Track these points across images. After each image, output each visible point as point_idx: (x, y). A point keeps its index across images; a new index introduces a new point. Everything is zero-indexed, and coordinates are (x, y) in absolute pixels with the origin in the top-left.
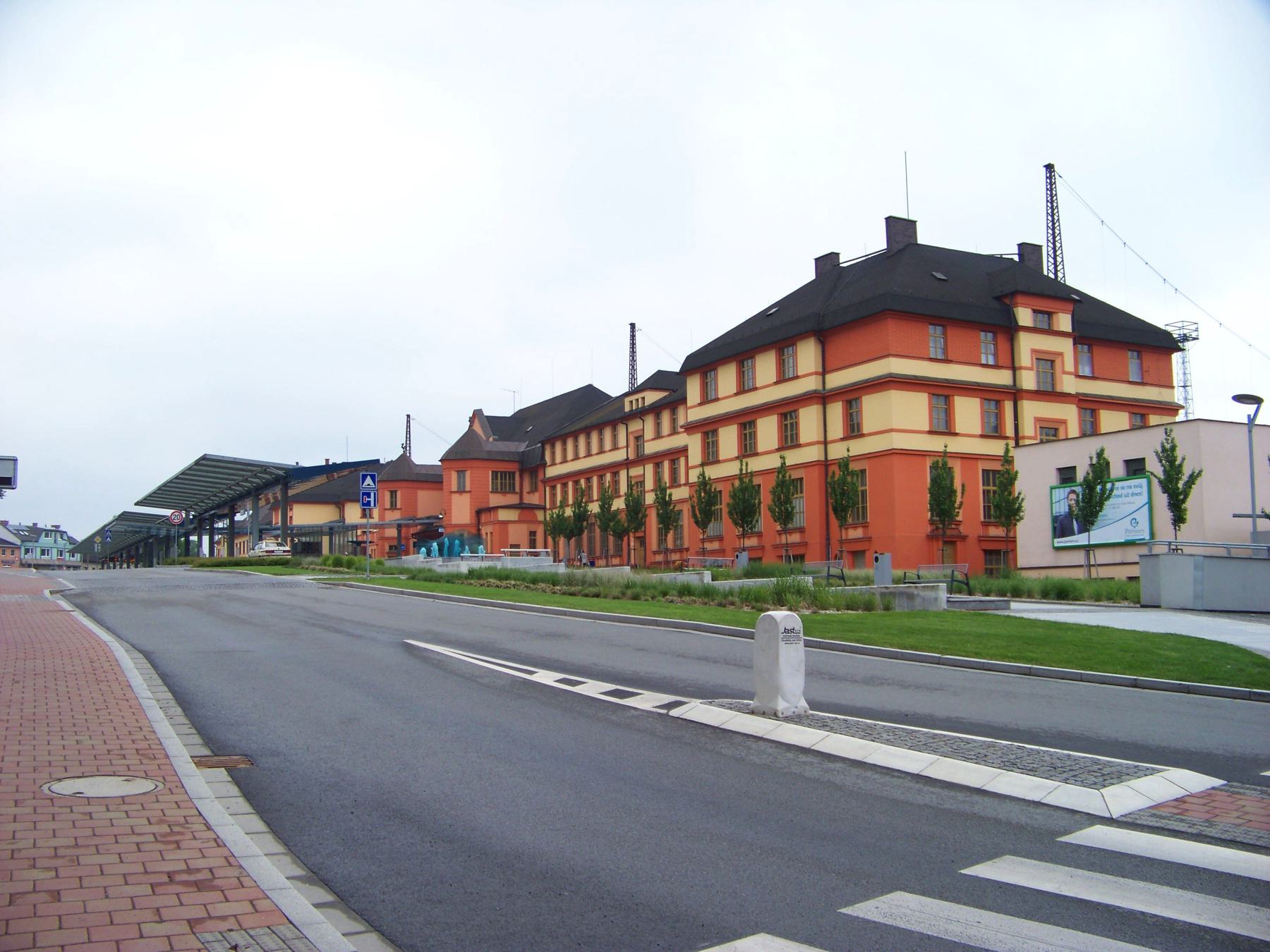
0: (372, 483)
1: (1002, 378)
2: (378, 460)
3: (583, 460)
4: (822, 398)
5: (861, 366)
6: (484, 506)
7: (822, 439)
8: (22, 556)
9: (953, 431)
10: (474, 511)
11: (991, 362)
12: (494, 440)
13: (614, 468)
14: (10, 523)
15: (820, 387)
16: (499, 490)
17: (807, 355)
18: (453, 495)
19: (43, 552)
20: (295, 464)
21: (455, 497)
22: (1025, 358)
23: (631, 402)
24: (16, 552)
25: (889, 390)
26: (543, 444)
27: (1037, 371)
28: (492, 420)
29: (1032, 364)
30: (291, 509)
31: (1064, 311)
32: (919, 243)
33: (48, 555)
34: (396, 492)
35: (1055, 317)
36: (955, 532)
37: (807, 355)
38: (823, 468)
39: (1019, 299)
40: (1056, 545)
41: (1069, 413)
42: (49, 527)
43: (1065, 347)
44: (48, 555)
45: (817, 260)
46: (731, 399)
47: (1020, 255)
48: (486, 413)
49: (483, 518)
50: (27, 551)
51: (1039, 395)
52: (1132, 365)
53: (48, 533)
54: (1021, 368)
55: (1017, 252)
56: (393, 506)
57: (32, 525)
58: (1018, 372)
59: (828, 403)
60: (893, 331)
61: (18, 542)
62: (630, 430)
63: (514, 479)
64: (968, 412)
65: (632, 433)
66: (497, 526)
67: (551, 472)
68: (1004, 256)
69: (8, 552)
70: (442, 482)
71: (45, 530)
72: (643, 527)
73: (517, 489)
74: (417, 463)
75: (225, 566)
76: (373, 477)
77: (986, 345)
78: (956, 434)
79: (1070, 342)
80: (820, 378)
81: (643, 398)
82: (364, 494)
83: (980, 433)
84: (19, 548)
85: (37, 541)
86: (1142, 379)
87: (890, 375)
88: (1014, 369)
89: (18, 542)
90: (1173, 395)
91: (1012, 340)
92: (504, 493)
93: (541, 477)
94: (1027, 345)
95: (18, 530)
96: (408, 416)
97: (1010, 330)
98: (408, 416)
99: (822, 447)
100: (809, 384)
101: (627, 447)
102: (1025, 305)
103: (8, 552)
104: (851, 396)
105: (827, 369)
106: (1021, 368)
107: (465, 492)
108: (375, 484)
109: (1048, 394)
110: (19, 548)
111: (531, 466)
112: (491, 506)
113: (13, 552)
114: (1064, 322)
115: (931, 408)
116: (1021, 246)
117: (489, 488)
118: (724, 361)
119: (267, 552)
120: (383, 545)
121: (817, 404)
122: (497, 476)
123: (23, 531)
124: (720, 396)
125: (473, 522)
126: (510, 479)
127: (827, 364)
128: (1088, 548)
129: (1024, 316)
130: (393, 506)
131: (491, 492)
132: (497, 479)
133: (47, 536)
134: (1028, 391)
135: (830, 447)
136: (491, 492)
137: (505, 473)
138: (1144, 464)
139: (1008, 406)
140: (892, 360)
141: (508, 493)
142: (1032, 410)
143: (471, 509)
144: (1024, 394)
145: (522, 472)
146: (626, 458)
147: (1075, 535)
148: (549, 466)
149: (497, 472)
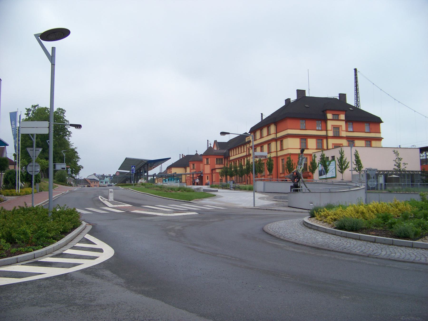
0: (134, 168)
1: (323, 133)
3: (235, 156)
4: (276, 140)
6: (213, 168)
7: (276, 151)
8: (100, 184)
9: (307, 148)
10: (211, 170)
11: (320, 129)
12: (219, 149)
13: (243, 157)
14: (96, 174)
15: (275, 137)
16: (218, 163)
17: (273, 128)
18: (205, 165)
19: (106, 183)
21: (206, 166)
22: (329, 127)
23: (247, 139)
24: (98, 183)
25: (288, 138)
26: (229, 150)
27: (334, 131)
28: (219, 143)
29: (332, 129)
30: (171, 169)
31: (342, 114)
32: (306, 96)
33: (107, 183)
34: (194, 164)
35: (339, 116)
36: (307, 175)
37: (273, 128)
38: (276, 158)
39: (328, 112)
40: (320, 178)
41: (344, 142)
42: (108, 175)
43: (343, 124)
44: (107, 183)
45: (285, 100)
46: (266, 137)
47: (339, 97)
48: (218, 141)
49: (213, 171)
50: (101, 182)
51: (333, 137)
52: (367, 127)
53: (107, 177)
54: (328, 130)
55: (339, 96)
56: (194, 169)
57: (103, 175)
58: (328, 131)
59: (300, 139)
60: (289, 123)
61: (98, 180)
62: (247, 147)
63: (222, 160)
64: (312, 143)
65: (247, 147)
66: (216, 174)
67: (231, 158)
68: (335, 98)
69: (96, 183)
70: (202, 161)
71: (106, 176)
72: (30, 184)
73: (223, 163)
75: (124, 186)
76: (134, 167)
77: (319, 125)
78: (308, 149)
79: (344, 122)
80: (275, 134)
81: (250, 138)
82: (132, 170)
83: (316, 148)
84: (99, 181)
85: (104, 179)
86: (370, 131)
87: (288, 134)
88: (327, 130)
89: (98, 180)
90: (380, 135)
91: (326, 123)
92: (220, 164)
93: (229, 160)
94: (330, 124)
95: (99, 176)
96: (208, 140)
97: (325, 120)
98: (208, 140)
99: (276, 153)
100: (272, 136)
101: (246, 151)
103: (96, 183)
104: (281, 139)
105: (277, 132)
106: (328, 130)
107: (208, 164)
108: (134, 168)
109: (337, 136)
110: (99, 181)
111: (227, 156)
112: (216, 168)
113: (94, 182)
114: (342, 117)
116: (339, 94)
117: (215, 163)
118: (264, 126)
119: (141, 182)
120: (191, 180)
121: (274, 141)
122: (220, 160)
123: (100, 176)
124: (264, 136)
125: (211, 173)
126: (221, 160)
127: (277, 130)
128: (326, 179)
129: (329, 116)
130: (194, 169)
131: (216, 164)
132: (217, 160)
133: (107, 178)
134: (330, 137)
135: (278, 153)
136: (216, 164)
137: (220, 159)
138: (334, 157)
139: (325, 141)
140: (289, 130)
141: (221, 164)
142: (331, 142)
143: (210, 169)
144: (329, 137)
145: (225, 158)
146: (246, 154)
147: (323, 175)
148: (231, 157)
149: (217, 159)
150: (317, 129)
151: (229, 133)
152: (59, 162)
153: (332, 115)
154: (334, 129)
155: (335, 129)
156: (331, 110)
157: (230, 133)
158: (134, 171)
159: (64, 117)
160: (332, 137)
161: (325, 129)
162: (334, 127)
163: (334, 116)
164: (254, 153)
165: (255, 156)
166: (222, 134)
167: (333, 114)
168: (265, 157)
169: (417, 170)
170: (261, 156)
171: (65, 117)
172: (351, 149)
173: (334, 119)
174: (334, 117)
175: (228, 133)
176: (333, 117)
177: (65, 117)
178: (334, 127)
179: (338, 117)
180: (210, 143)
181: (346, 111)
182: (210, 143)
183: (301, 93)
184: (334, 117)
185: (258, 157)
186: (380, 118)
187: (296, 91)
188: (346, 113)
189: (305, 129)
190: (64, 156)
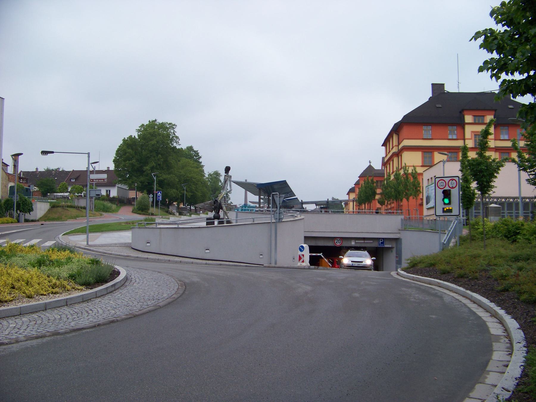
1: (459, 143)
2: (370, 168)
5: (443, 140)
11: (455, 137)
20: (245, 181)
22: (468, 134)
25: (404, 152)
35: (485, 117)
39: (465, 112)
68: (492, 92)
74: (376, 169)
77: (452, 132)
82: (158, 197)
83: (421, 165)
88: (464, 139)
91: (464, 129)
94: (469, 130)
97: (462, 125)
102: (469, 114)
115: (488, 151)
129: (468, 118)
150: (450, 137)
151: (53, 152)
152: (226, 185)
153: (473, 117)
154: (475, 138)
155: (477, 136)
156: (470, 110)
157: (54, 151)
158: (160, 198)
159: (175, 133)
160: (472, 148)
161: (463, 138)
162: (475, 135)
163: (477, 118)
164: (89, 176)
165: (91, 180)
166: (43, 154)
167: (474, 116)
168: (104, 180)
169: (500, 196)
170: (99, 180)
171: (176, 132)
172: (444, 166)
173: (477, 122)
174: (477, 119)
175: (52, 152)
176: (475, 120)
177: (176, 132)
178: (475, 135)
179: (483, 120)
180: (370, 161)
181: (495, 110)
182: (370, 161)
183: (438, 88)
184: (477, 119)
185: (94, 180)
186: (395, 124)
187: (431, 86)
188: (496, 113)
189: (431, 138)
190: (155, 180)
